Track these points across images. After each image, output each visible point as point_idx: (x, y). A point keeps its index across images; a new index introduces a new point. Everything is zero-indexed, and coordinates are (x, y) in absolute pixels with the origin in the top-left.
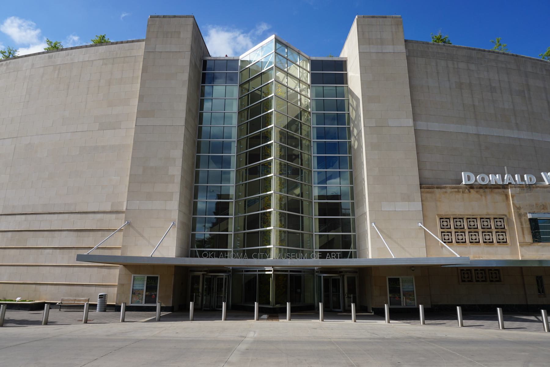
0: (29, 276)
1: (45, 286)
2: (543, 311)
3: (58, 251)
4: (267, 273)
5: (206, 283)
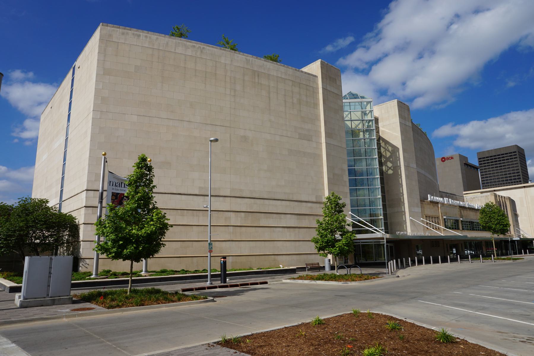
0: (267, 248)
1: (281, 256)
2: (394, 260)
3: (286, 229)
4: (381, 243)
5: (496, 249)
